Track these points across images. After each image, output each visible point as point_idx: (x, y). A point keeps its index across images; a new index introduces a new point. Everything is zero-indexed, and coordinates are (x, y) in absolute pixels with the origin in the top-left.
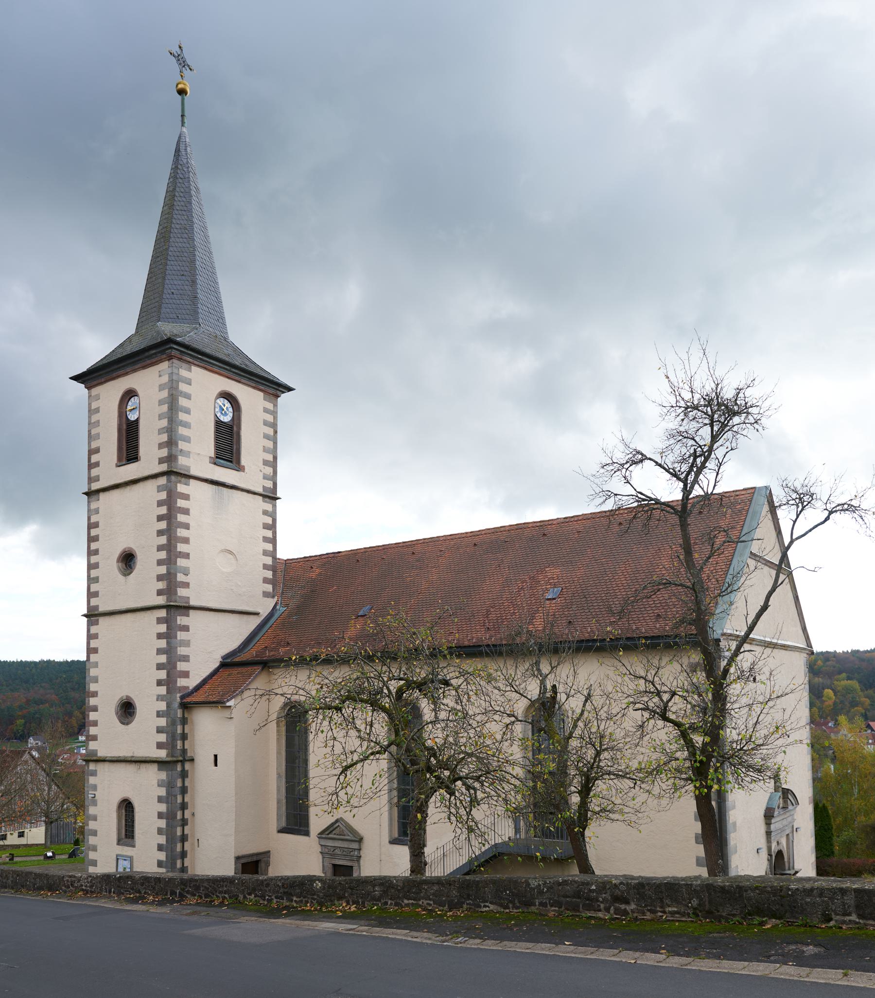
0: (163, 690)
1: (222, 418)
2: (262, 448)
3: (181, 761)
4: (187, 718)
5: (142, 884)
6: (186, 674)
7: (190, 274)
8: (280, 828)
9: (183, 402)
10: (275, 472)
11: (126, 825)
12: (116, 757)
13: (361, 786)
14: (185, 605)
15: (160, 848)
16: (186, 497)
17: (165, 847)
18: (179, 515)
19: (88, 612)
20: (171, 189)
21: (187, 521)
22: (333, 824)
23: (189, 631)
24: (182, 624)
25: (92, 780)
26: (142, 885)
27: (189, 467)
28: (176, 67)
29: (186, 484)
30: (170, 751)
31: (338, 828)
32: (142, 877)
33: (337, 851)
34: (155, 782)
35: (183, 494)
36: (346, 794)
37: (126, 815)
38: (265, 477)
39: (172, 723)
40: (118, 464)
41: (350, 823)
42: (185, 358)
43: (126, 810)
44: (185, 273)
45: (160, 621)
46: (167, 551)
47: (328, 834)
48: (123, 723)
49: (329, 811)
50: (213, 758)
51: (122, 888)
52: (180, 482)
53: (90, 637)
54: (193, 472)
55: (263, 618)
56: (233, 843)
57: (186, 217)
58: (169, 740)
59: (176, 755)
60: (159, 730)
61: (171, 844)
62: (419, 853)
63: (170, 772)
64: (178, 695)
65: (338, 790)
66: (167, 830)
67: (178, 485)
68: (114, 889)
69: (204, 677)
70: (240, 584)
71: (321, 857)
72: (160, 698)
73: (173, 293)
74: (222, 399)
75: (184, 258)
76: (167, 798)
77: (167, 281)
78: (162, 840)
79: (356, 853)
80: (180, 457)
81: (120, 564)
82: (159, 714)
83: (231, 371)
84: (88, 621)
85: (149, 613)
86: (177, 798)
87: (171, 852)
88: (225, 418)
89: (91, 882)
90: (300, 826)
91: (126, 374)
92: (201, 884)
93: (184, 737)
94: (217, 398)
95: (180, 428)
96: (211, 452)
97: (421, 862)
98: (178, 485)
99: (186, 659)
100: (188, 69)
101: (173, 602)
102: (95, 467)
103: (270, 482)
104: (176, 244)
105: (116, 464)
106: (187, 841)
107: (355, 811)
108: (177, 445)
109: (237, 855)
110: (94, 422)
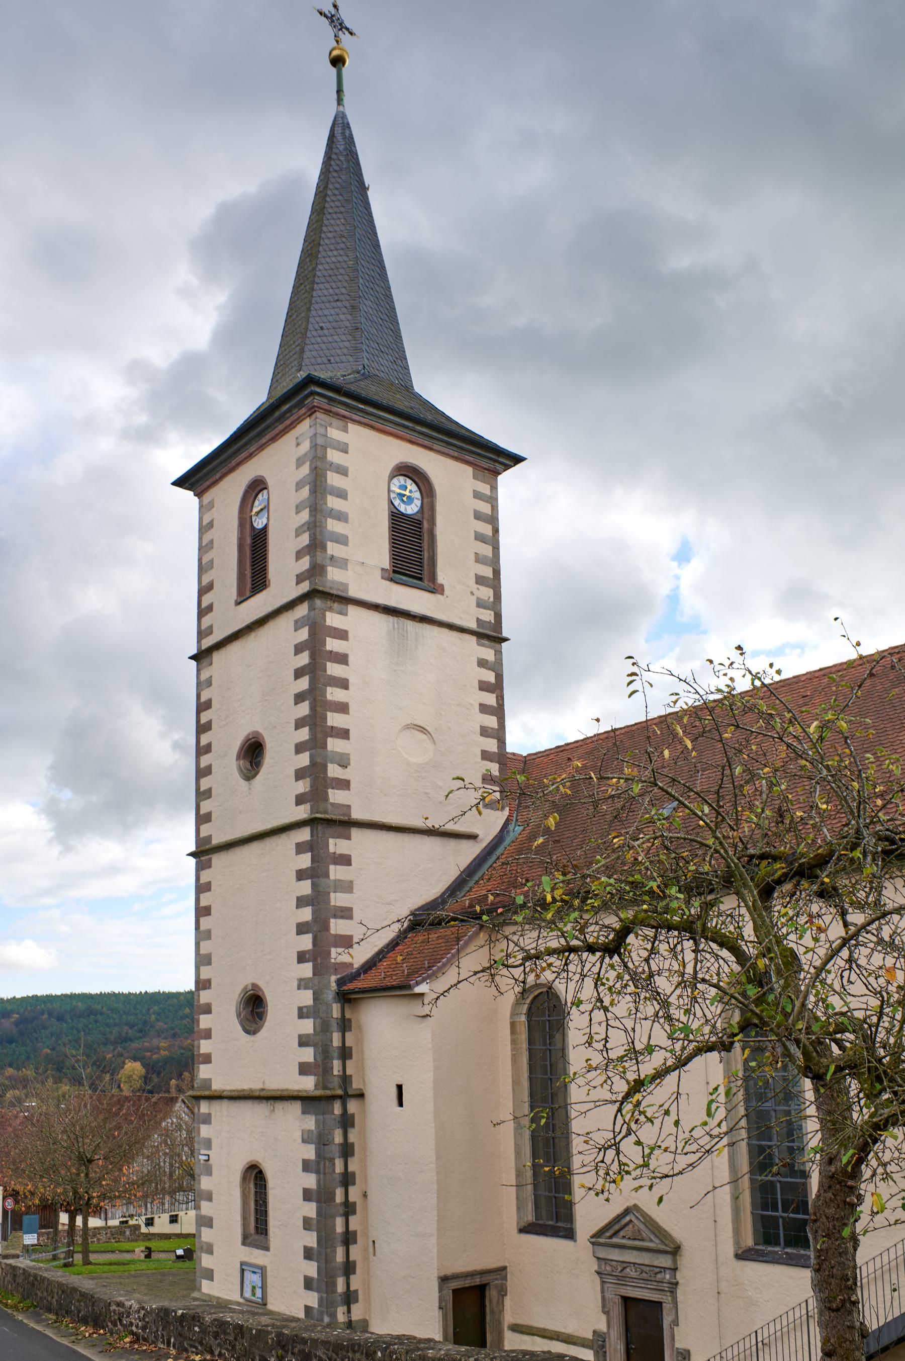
0: (307, 970)
1: (402, 508)
2: (473, 557)
3: (340, 1097)
4: (350, 1020)
5: (216, 1335)
6: (346, 942)
7: (348, 298)
8: (522, 1224)
9: (333, 479)
10: (498, 596)
11: (256, 1210)
12: (238, 1091)
13: (677, 1123)
14: (342, 818)
15: (308, 1254)
16: (342, 635)
17: (315, 1252)
18: (329, 664)
19: (196, 848)
20: (321, 189)
21: (344, 676)
22: (619, 1218)
23: (350, 865)
24: (339, 852)
25: (205, 1131)
26: (216, 1339)
27: (346, 585)
28: (330, 31)
29: (340, 613)
30: (321, 1079)
31: (631, 1226)
32: (215, 1320)
33: (630, 1272)
34: (298, 1135)
35: (335, 629)
36: (638, 1143)
37: (256, 1192)
38: (480, 604)
39: (324, 1028)
40: (239, 601)
41: (654, 1216)
42: (335, 409)
43: (256, 1184)
44: (341, 297)
45: (300, 848)
46: (310, 725)
47: (611, 1237)
48: (247, 1032)
49: (599, 1187)
50: (394, 1091)
51: (185, 1338)
52: (331, 609)
53: (202, 888)
54: (353, 593)
55: (484, 845)
56: (435, 1250)
57: (342, 221)
58: (318, 1059)
59: (331, 1086)
60: (303, 1042)
61: (326, 1248)
62: (843, 1302)
63: (321, 1117)
64: (333, 978)
65: (617, 1140)
66: (318, 1221)
67: (328, 614)
68: (175, 1338)
69: (380, 947)
70: (441, 784)
71: (598, 1281)
72: (303, 984)
73: (322, 328)
74: (402, 478)
75: (340, 277)
76: (318, 1163)
77: (314, 313)
78: (311, 1239)
79: (668, 1276)
80: (329, 569)
81: (242, 762)
82: (302, 1013)
83: (415, 431)
84: (197, 863)
85: (284, 836)
86: (334, 1164)
87: (327, 1262)
88: (408, 508)
89: (144, 1319)
90: (557, 1221)
91: (251, 456)
92: (313, 1351)
93: (345, 1054)
94: (392, 477)
95: (329, 521)
96: (384, 560)
97: (851, 1327)
98: (328, 614)
99: (346, 913)
100: (347, 33)
101: (321, 813)
102: (206, 614)
103: (489, 612)
104: (328, 260)
105: (236, 601)
106: (355, 1242)
107: (662, 1187)
108: (324, 548)
109: (442, 1274)
110: (207, 544)
